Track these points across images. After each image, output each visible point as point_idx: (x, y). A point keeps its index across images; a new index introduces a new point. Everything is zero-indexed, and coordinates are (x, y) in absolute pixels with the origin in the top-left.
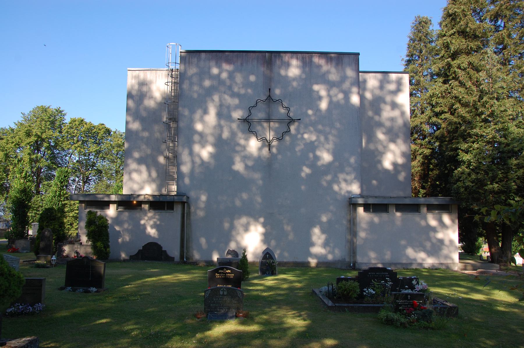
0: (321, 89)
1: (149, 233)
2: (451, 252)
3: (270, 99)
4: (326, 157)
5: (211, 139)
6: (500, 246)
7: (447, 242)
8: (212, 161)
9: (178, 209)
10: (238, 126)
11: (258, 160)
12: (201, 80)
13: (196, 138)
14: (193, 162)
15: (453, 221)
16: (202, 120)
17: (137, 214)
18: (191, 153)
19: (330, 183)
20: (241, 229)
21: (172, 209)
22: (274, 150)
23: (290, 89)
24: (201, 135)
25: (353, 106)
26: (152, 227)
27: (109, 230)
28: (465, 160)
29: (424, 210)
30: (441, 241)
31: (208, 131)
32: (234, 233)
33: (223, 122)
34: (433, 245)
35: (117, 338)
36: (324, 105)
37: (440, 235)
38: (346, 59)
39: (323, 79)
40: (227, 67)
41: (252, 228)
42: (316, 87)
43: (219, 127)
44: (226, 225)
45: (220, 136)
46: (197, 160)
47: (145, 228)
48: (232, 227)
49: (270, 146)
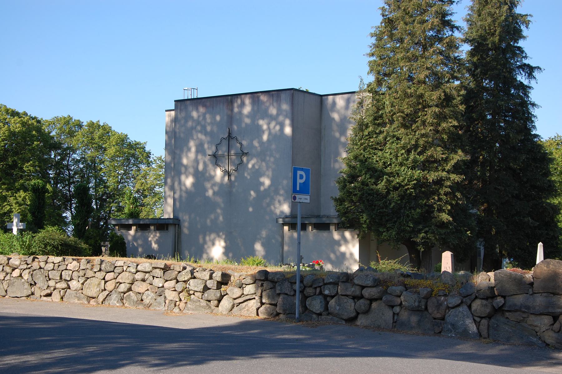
0: (263, 123)
1: (154, 247)
2: (351, 265)
3: (230, 137)
4: (267, 182)
5: (191, 170)
6: (540, 245)
7: (348, 255)
8: (193, 189)
9: (171, 229)
10: (210, 160)
11: (221, 185)
12: (186, 121)
13: (183, 170)
14: (181, 190)
15: (353, 237)
16: (187, 157)
17: (146, 233)
18: (180, 182)
19: (269, 205)
20: (210, 243)
21: (167, 229)
22: (233, 178)
23: (243, 125)
24: (186, 167)
25: (286, 136)
26: (155, 243)
27: (126, 245)
28: (531, 80)
29: (332, 228)
30: (343, 255)
31: (190, 164)
32: (206, 246)
33: (200, 157)
34: (337, 257)
35: (525, 25)
36: (265, 137)
37: (343, 249)
38: (283, 95)
39: (266, 115)
40: (202, 110)
41: (217, 243)
42: (261, 122)
43: (197, 161)
44: (201, 241)
45: (197, 168)
46: (183, 188)
47: (151, 244)
48: (205, 242)
49: (229, 176)
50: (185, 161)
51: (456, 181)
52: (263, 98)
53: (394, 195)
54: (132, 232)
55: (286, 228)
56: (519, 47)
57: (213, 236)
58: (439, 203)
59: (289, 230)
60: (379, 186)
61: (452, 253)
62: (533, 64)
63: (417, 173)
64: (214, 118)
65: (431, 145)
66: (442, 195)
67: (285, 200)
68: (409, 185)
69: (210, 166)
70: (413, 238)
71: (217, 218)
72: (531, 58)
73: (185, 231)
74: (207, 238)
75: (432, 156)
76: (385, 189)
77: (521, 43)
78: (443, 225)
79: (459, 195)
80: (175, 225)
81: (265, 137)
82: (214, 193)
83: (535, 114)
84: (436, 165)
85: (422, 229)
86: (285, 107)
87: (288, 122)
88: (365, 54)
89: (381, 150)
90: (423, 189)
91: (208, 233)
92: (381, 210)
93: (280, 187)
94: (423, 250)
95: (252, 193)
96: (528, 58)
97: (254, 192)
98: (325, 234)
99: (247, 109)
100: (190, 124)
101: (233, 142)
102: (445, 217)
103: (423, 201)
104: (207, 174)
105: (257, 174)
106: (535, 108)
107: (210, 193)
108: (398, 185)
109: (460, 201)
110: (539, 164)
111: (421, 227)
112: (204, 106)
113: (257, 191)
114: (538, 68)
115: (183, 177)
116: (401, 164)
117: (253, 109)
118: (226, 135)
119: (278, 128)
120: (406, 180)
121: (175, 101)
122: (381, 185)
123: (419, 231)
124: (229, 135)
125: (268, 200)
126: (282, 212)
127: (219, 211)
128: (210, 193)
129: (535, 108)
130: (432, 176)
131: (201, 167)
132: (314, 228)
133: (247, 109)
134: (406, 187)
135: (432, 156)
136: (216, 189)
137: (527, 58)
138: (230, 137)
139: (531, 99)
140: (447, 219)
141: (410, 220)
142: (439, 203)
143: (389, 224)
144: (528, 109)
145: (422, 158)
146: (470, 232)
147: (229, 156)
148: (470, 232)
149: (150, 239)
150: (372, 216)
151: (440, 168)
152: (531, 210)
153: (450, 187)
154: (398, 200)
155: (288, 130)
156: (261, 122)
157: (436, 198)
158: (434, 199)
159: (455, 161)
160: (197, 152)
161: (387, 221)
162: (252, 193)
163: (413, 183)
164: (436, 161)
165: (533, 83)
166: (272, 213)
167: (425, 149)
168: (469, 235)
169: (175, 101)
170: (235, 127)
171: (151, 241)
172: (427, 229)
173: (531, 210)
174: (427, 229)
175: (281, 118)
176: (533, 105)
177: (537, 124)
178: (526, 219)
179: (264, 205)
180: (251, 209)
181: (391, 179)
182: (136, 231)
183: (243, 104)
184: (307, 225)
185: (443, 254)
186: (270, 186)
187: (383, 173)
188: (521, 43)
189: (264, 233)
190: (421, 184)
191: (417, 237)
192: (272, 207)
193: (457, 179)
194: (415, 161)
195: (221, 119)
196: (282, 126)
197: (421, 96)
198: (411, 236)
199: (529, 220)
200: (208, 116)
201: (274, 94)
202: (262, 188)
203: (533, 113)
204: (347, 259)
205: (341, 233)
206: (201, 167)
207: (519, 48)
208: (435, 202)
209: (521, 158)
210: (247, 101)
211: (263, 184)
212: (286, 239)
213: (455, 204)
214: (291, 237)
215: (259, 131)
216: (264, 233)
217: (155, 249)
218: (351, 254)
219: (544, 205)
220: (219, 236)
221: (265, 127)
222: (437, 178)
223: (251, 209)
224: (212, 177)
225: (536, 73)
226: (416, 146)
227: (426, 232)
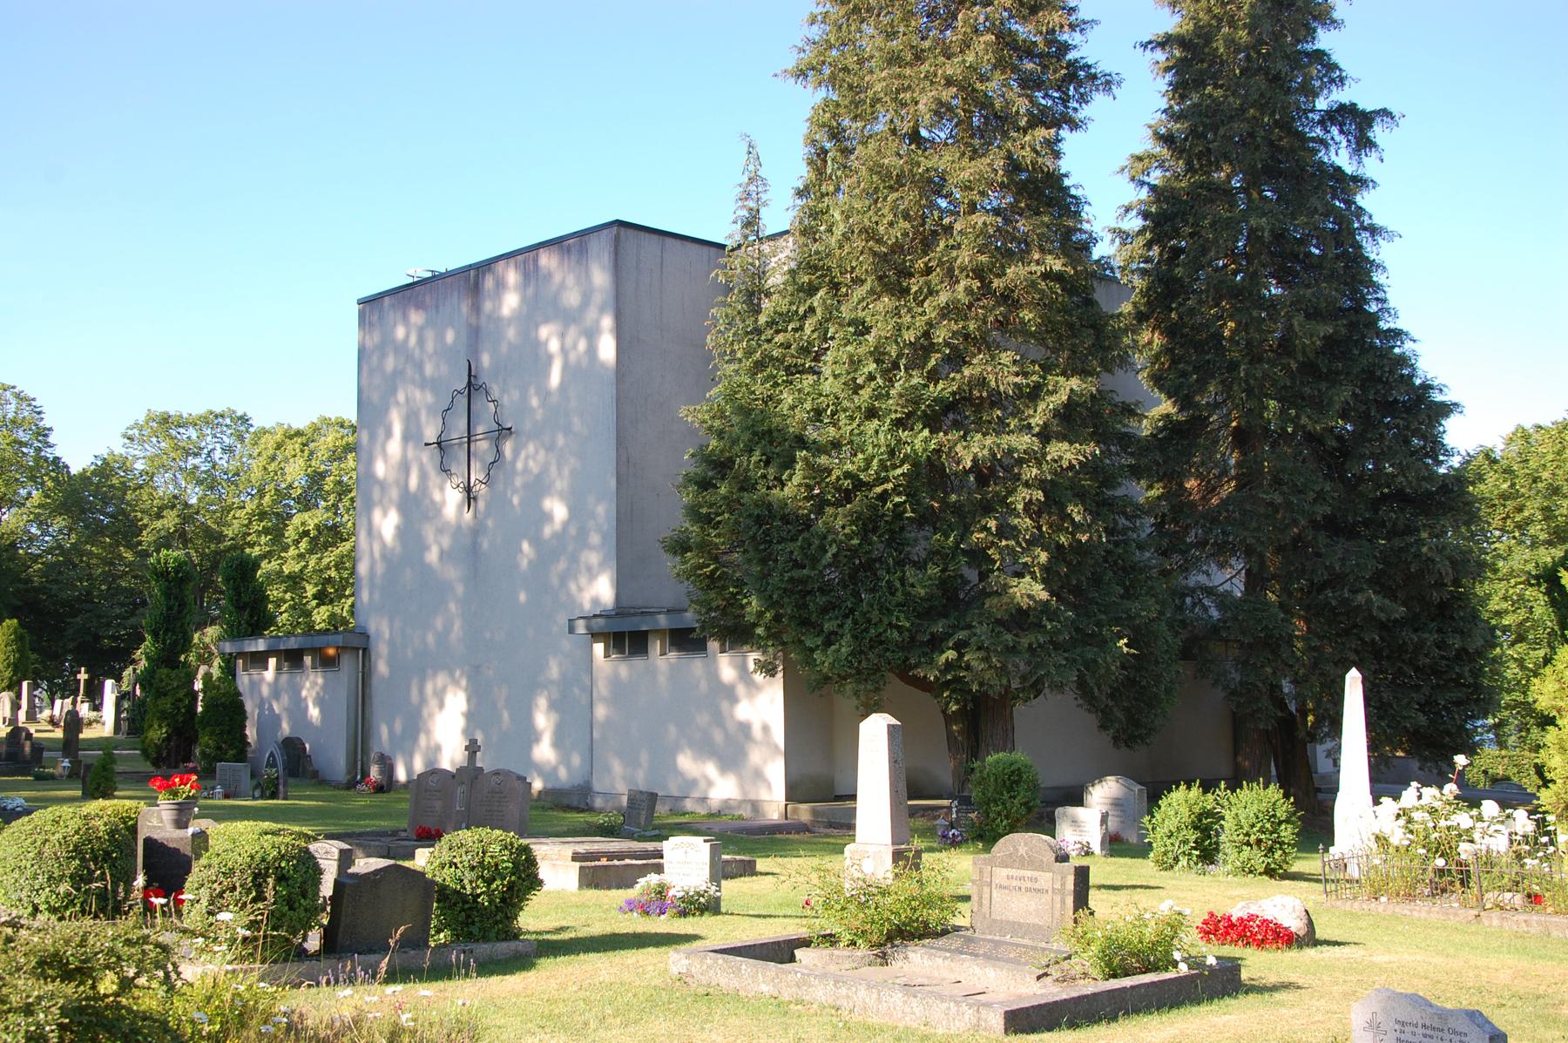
4: (558, 510)
5: (394, 493)
7: (757, 732)
9: (347, 662)
13: (376, 494)
19: (564, 579)
20: (433, 703)
25: (603, 365)
30: (745, 728)
31: (391, 478)
32: (425, 712)
36: (555, 378)
40: (416, 317)
43: (405, 467)
48: (423, 700)
50: (380, 469)
51: (1065, 464)
52: (546, 260)
53: (839, 520)
54: (269, 675)
55: (599, 648)
56: (1318, 51)
57: (441, 679)
58: (1004, 543)
59: (607, 655)
60: (788, 491)
61: (894, 722)
62: (1366, 104)
63: (920, 440)
64: (440, 337)
65: (983, 342)
66: (1018, 516)
67: (603, 565)
68: (887, 480)
69: (434, 477)
70: (916, 666)
71: (448, 628)
72: (1357, 81)
73: (382, 667)
74: (429, 688)
75: (983, 382)
76: (805, 498)
77: (1325, 40)
78: (1022, 618)
79: (1076, 512)
80: (358, 649)
81: (555, 378)
82: (442, 554)
83: (1378, 260)
84: (999, 412)
85: (947, 636)
86: (600, 277)
87: (607, 322)
88: (779, 72)
89: (812, 371)
90: (953, 497)
91: (430, 671)
92: (796, 573)
93: (591, 523)
94: (954, 708)
95: (525, 546)
96: (1347, 82)
97: (530, 545)
98: (696, 664)
99: (511, 302)
100: (390, 363)
101: (479, 402)
102: (1029, 590)
103: (947, 537)
104: (427, 501)
105: (538, 488)
106: (1379, 239)
107: (433, 556)
108: (847, 483)
109: (1084, 533)
110: (1402, 418)
111: (939, 627)
112: (420, 306)
113: (536, 541)
114: (1385, 113)
115: (377, 515)
116: (871, 413)
117: (524, 300)
118: (462, 384)
119: (582, 345)
120: (875, 461)
121: (361, 302)
122: (793, 488)
123: (936, 644)
124: (469, 383)
125: (562, 565)
126: (596, 601)
127: (452, 607)
128: (433, 556)
129: (1379, 239)
130: (972, 449)
131: (413, 482)
132: (672, 644)
133: (511, 302)
134: (879, 490)
135: (983, 382)
136: (446, 542)
137: (1343, 85)
138: (473, 386)
139: (1370, 217)
140: (1030, 596)
141: (899, 605)
142: (1004, 543)
143: (830, 619)
144: (1358, 247)
145: (942, 389)
146: (1125, 641)
147: (469, 443)
148: (1125, 641)
149: (304, 693)
150: (771, 597)
151: (1013, 423)
152: (1380, 566)
153: (1041, 484)
154: (849, 537)
155: (607, 349)
156: (544, 332)
157: (992, 524)
158: (985, 528)
159: (1063, 397)
160: (406, 438)
161: (824, 610)
162: (525, 546)
163: (899, 471)
164: (996, 399)
165: (1370, 166)
166: (572, 602)
167: (957, 359)
168: (1125, 650)
169: (361, 302)
170: (485, 360)
171: (306, 699)
172: (961, 635)
173: (1380, 566)
174: (961, 635)
175: (592, 314)
176: (1374, 231)
177: (1394, 298)
178: (1360, 598)
179: (555, 581)
180: (522, 597)
181: (823, 460)
182: (279, 668)
183: (501, 285)
184: (650, 638)
185: (861, 725)
186: (566, 525)
187: (801, 442)
188: (1325, 40)
189: (554, 671)
190: (931, 472)
191: (931, 662)
192: (573, 587)
193: (1068, 456)
194: (913, 398)
195: (457, 338)
196: (592, 335)
197: (855, 118)
198: (907, 659)
199: (1369, 601)
200: (430, 335)
201: (571, 245)
202: (547, 531)
203: (1372, 256)
204: (755, 742)
205: (739, 660)
206: (413, 482)
207: (1320, 56)
208: (991, 538)
209: (1336, 398)
210: (512, 276)
211: (548, 517)
212: (602, 688)
213: (1070, 545)
214: (615, 682)
215: (537, 360)
216: (554, 671)
217: (314, 720)
218: (766, 729)
219: (1424, 549)
220: (456, 683)
221: (554, 346)
222: (994, 455)
223: (522, 597)
224: (437, 509)
225: (1378, 132)
226: (924, 347)
227: (960, 647)
